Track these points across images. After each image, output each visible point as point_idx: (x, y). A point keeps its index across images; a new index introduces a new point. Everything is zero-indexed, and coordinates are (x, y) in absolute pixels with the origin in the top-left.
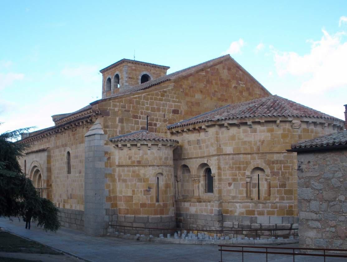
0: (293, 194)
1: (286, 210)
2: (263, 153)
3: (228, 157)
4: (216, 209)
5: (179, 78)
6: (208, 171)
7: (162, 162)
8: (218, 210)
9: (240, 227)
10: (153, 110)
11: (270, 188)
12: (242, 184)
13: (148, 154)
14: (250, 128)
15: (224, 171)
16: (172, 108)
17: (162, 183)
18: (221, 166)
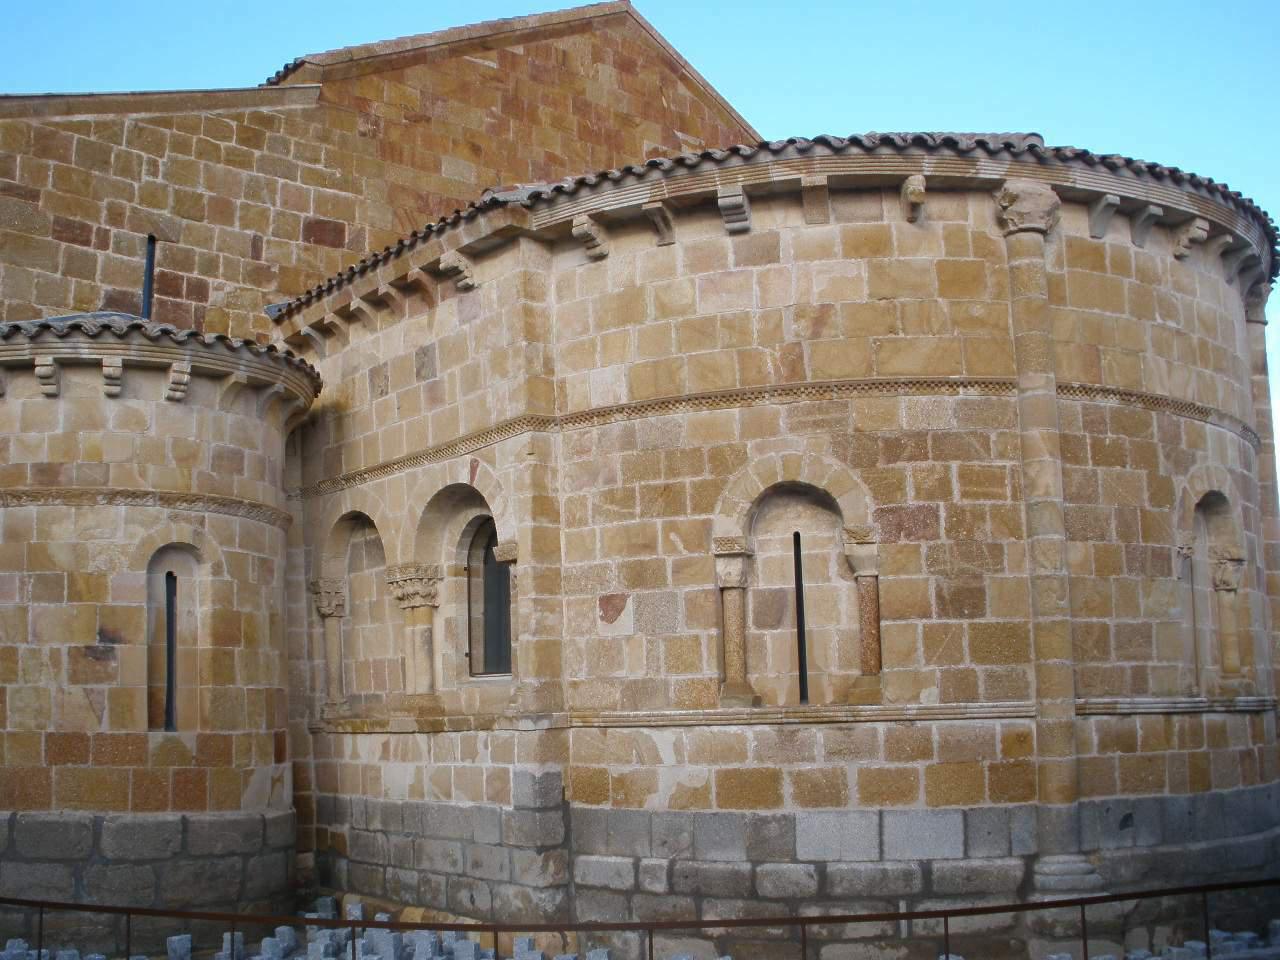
0: (1032, 656)
1: (987, 763)
2: (823, 389)
3: (595, 432)
4: (525, 767)
5: (351, 60)
6: (483, 532)
7: (194, 483)
8: (538, 775)
9: (682, 885)
10: (188, 206)
11: (878, 619)
12: (691, 601)
13: (103, 426)
14: (733, 233)
15: (569, 524)
16: (302, 210)
17: (197, 611)
18: (556, 490)
